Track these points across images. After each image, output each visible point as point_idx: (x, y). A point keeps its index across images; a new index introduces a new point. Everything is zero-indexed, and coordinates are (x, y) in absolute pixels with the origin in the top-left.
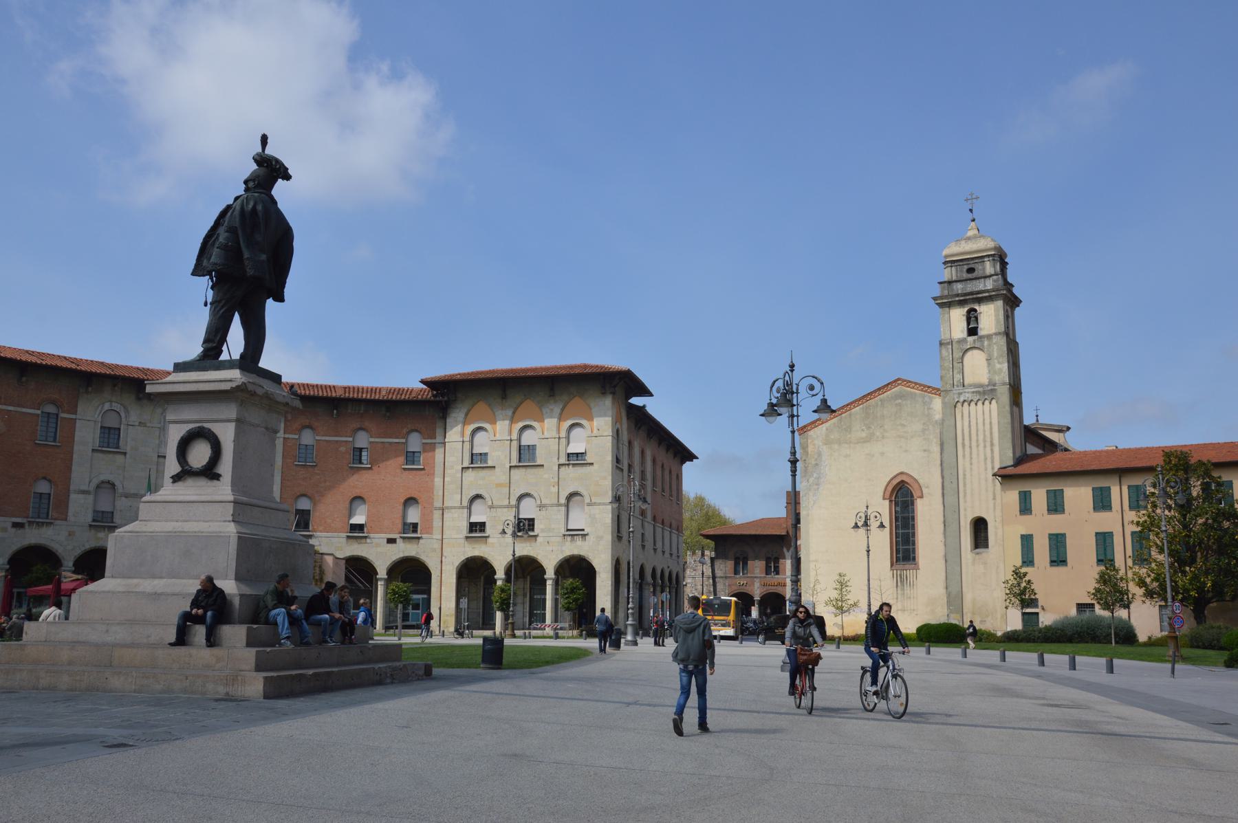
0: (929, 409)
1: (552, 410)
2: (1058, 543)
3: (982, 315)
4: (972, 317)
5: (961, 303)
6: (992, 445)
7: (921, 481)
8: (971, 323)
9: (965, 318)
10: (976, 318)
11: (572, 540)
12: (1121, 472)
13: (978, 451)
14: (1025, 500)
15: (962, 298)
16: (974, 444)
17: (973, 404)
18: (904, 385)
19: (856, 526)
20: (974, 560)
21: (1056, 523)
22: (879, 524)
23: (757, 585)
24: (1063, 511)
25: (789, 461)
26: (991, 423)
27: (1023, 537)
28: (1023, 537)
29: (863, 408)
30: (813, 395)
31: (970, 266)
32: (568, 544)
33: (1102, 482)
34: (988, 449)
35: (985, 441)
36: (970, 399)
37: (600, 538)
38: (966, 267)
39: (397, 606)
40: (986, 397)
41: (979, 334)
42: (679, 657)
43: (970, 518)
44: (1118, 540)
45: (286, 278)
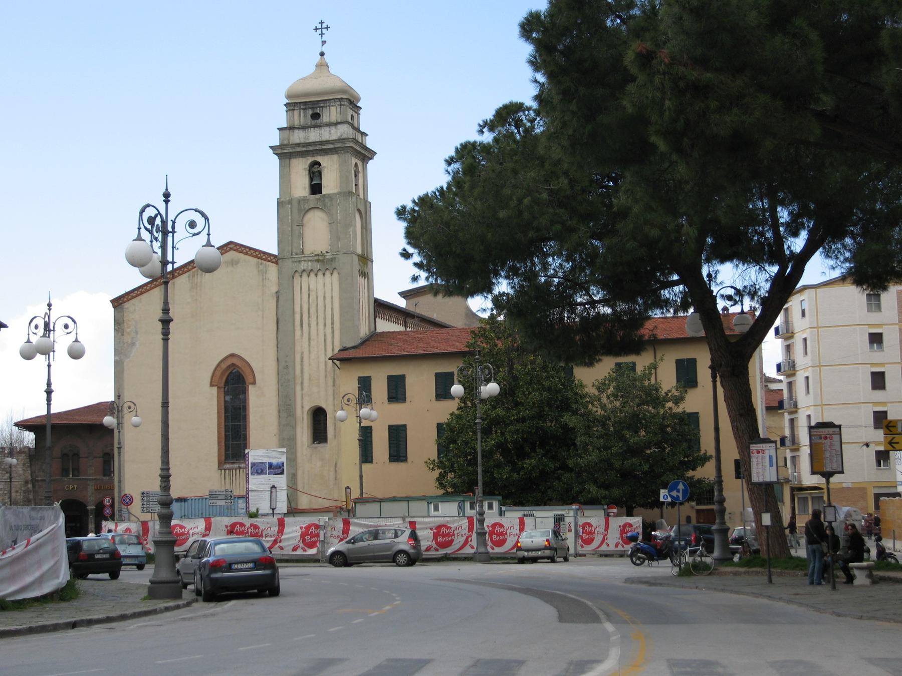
2: (398, 435)
3: (325, 169)
4: (315, 172)
5: (303, 154)
8: (315, 178)
9: (307, 172)
10: (320, 173)
14: (365, 384)
15: (304, 149)
21: (397, 414)
23: (91, 489)
24: (404, 400)
25: (159, 320)
26: (332, 297)
27: (874, 374)
28: (874, 374)
30: (194, 235)
36: (310, 268)
38: (310, 112)
40: (327, 267)
41: (323, 193)
43: (307, 408)
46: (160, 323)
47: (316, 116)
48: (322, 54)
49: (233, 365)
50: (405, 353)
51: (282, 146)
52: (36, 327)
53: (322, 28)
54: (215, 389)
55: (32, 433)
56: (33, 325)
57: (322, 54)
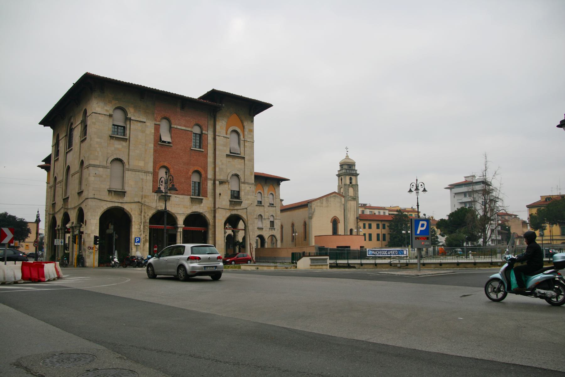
1: (266, 188)
2: (370, 235)
5: (349, 175)
6: (355, 211)
11: (272, 230)
12: (382, 221)
14: (364, 225)
19: (410, 191)
21: (370, 231)
22: (423, 189)
32: (271, 231)
34: (354, 212)
35: (353, 210)
37: (278, 230)
38: (349, 166)
42: (550, 199)
43: (350, 229)
45: (206, 94)
46: (419, 189)
47: (350, 167)
49: (335, 218)
51: (338, 174)
52: (413, 186)
53: (347, 148)
55: (242, 241)
56: (412, 185)
57: (347, 154)
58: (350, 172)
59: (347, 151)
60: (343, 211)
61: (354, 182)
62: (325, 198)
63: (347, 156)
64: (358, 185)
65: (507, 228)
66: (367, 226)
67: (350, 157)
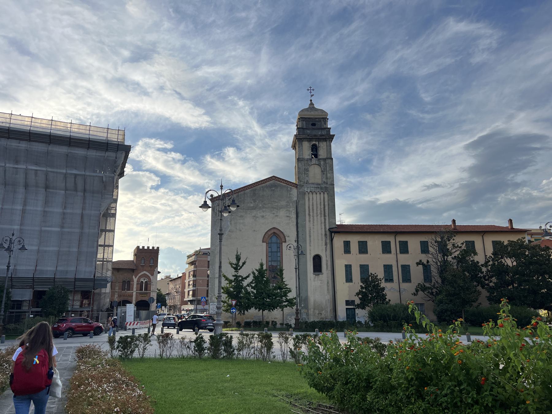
0: (290, 194)
5: (310, 140)
7: (285, 233)
13: (317, 218)
14: (347, 245)
16: (315, 215)
17: (314, 194)
18: (276, 180)
20: (315, 278)
27: (346, 266)
28: (346, 266)
29: (252, 190)
31: (313, 122)
33: (386, 238)
34: (323, 218)
39: (269, 337)
43: (313, 255)
44: (394, 269)
47: (314, 125)
48: (311, 101)
50: (382, 230)
54: (265, 244)
57: (311, 101)
58: (314, 132)
59: (312, 96)
60: (294, 216)
61: (322, 153)
62: (249, 190)
63: (312, 104)
64: (332, 159)
65: (544, 291)
66: (354, 247)
67: (316, 106)
